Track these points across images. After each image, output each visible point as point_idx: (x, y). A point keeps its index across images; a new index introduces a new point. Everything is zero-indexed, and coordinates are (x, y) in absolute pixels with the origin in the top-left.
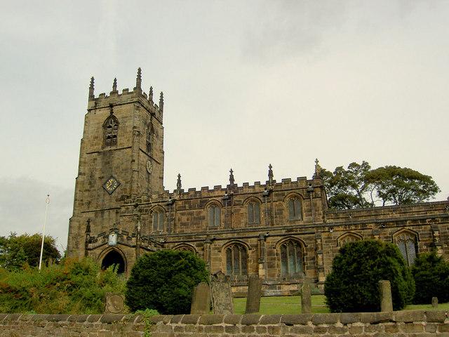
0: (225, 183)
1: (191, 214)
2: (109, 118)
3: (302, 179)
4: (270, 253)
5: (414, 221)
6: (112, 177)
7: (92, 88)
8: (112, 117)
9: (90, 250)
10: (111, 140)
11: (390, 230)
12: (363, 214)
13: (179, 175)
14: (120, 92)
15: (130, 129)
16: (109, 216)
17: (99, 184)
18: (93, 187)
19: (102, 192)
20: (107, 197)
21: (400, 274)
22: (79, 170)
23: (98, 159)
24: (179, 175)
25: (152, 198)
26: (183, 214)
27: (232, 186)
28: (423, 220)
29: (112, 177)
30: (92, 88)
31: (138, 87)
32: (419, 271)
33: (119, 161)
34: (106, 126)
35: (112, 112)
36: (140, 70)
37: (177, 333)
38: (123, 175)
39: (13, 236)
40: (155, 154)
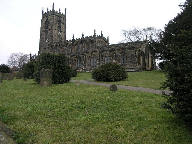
0: (81, 37)
3: (90, 37)
4: (74, 61)
5: (110, 50)
7: (43, 11)
10: (47, 27)
11: (103, 53)
12: (105, 47)
14: (49, 12)
15: (51, 23)
17: (45, 40)
20: (46, 44)
26: (62, 49)
27: (73, 39)
28: (112, 50)
30: (43, 11)
31: (53, 10)
32: (182, 45)
34: (46, 23)
35: (47, 18)
39: (178, 15)
40: (62, 30)
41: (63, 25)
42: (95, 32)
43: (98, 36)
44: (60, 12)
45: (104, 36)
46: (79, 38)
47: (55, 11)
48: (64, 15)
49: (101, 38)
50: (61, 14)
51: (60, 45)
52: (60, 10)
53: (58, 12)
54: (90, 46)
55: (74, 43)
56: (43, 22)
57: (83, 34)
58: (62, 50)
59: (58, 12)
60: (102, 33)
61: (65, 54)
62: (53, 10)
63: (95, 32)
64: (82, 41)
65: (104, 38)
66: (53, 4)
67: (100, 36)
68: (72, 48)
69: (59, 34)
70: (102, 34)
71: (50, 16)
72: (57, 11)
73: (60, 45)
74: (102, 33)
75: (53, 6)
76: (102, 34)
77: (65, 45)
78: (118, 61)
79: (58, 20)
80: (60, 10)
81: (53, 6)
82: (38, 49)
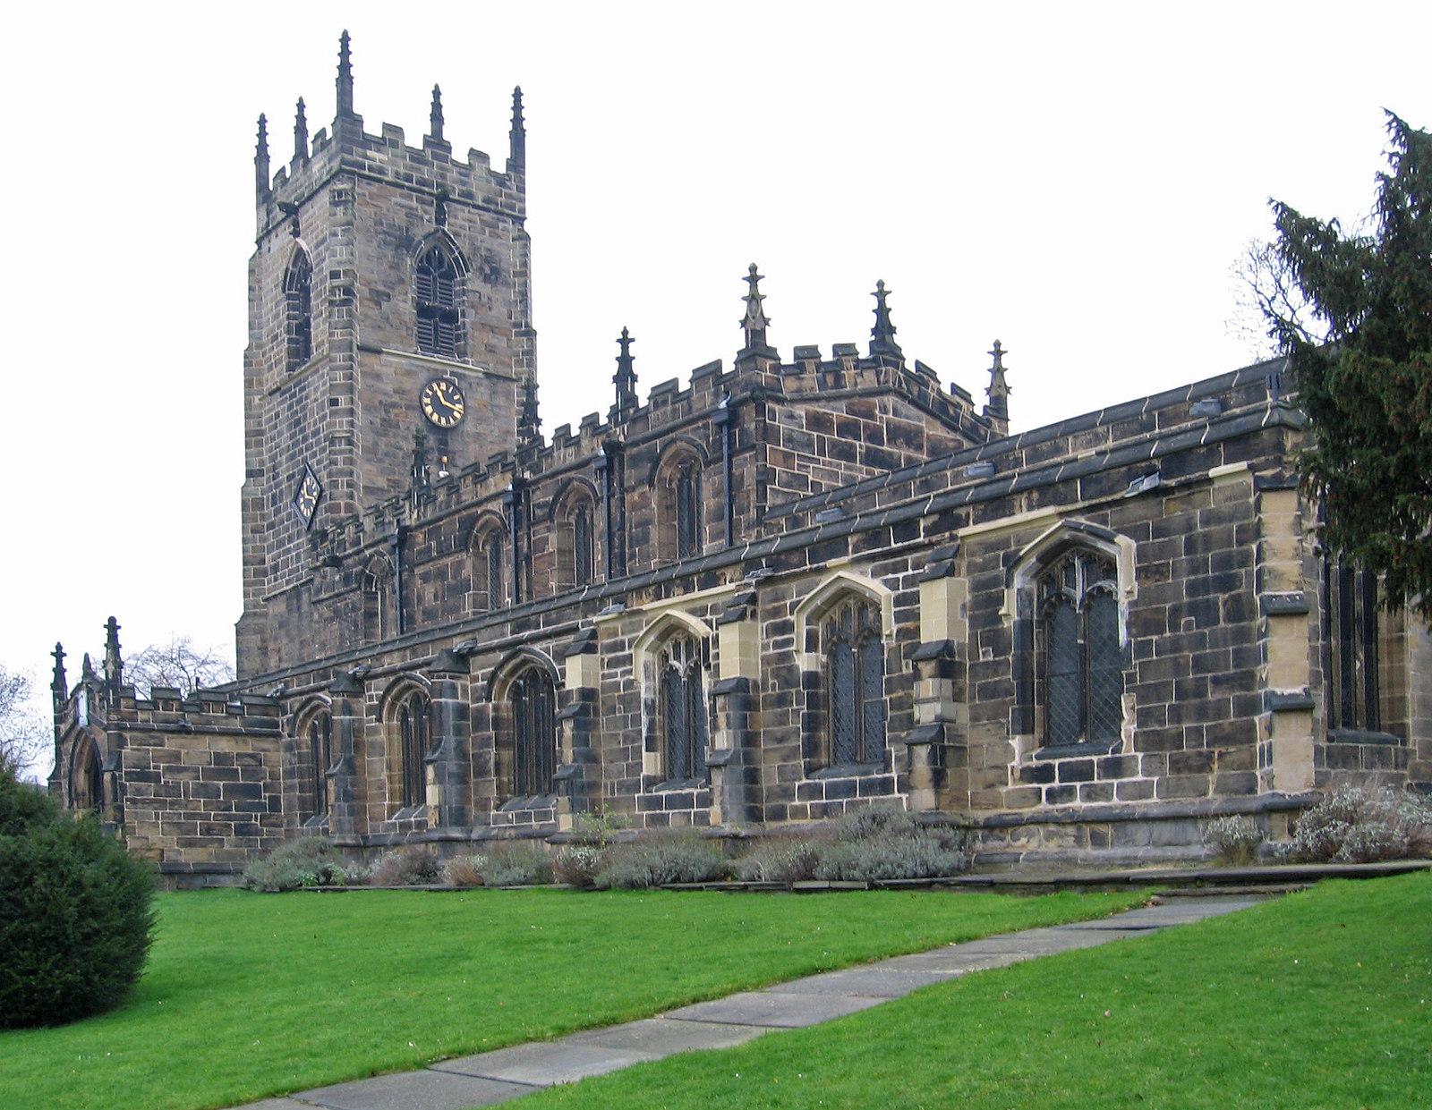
3: (708, 374)
26: (426, 578)
30: (262, 157)
31: (347, 116)
41: (486, 289)
42: (754, 299)
43: (806, 354)
44: (436, 142)
45: (913, 347)
46: (590, 422)
47: (373, 128)
48: (499, 165)
49: (869, 380)
50: (460, 155)
51: (405, 532)
52: (437, 117)
53: (414, 139)
54: (709, 502)
55: (541, 497)
56: (1175, 394)
57: (625, 361)
58: (429, 591)
59: (414, 139)
60: (882, 312)
61: (1362, 544)
62: (347, 116)
63: (754, 299)
64: (613, 449)
65: (925, 374)
66: (345, 53)
67: (844, 350)
68: (523, 561)
69: (445, 411)
70: (883, 329)
71: (324, 198)
72: (393, 133)
73: (405, 532)
74: (882, 312)
75: (345, 67)
76: (883, 329)
77: (451, 527)
78: (988, 692)
79: (418, 233)
80: (437, 117)
81: (345, 67)
82: (233, 606)
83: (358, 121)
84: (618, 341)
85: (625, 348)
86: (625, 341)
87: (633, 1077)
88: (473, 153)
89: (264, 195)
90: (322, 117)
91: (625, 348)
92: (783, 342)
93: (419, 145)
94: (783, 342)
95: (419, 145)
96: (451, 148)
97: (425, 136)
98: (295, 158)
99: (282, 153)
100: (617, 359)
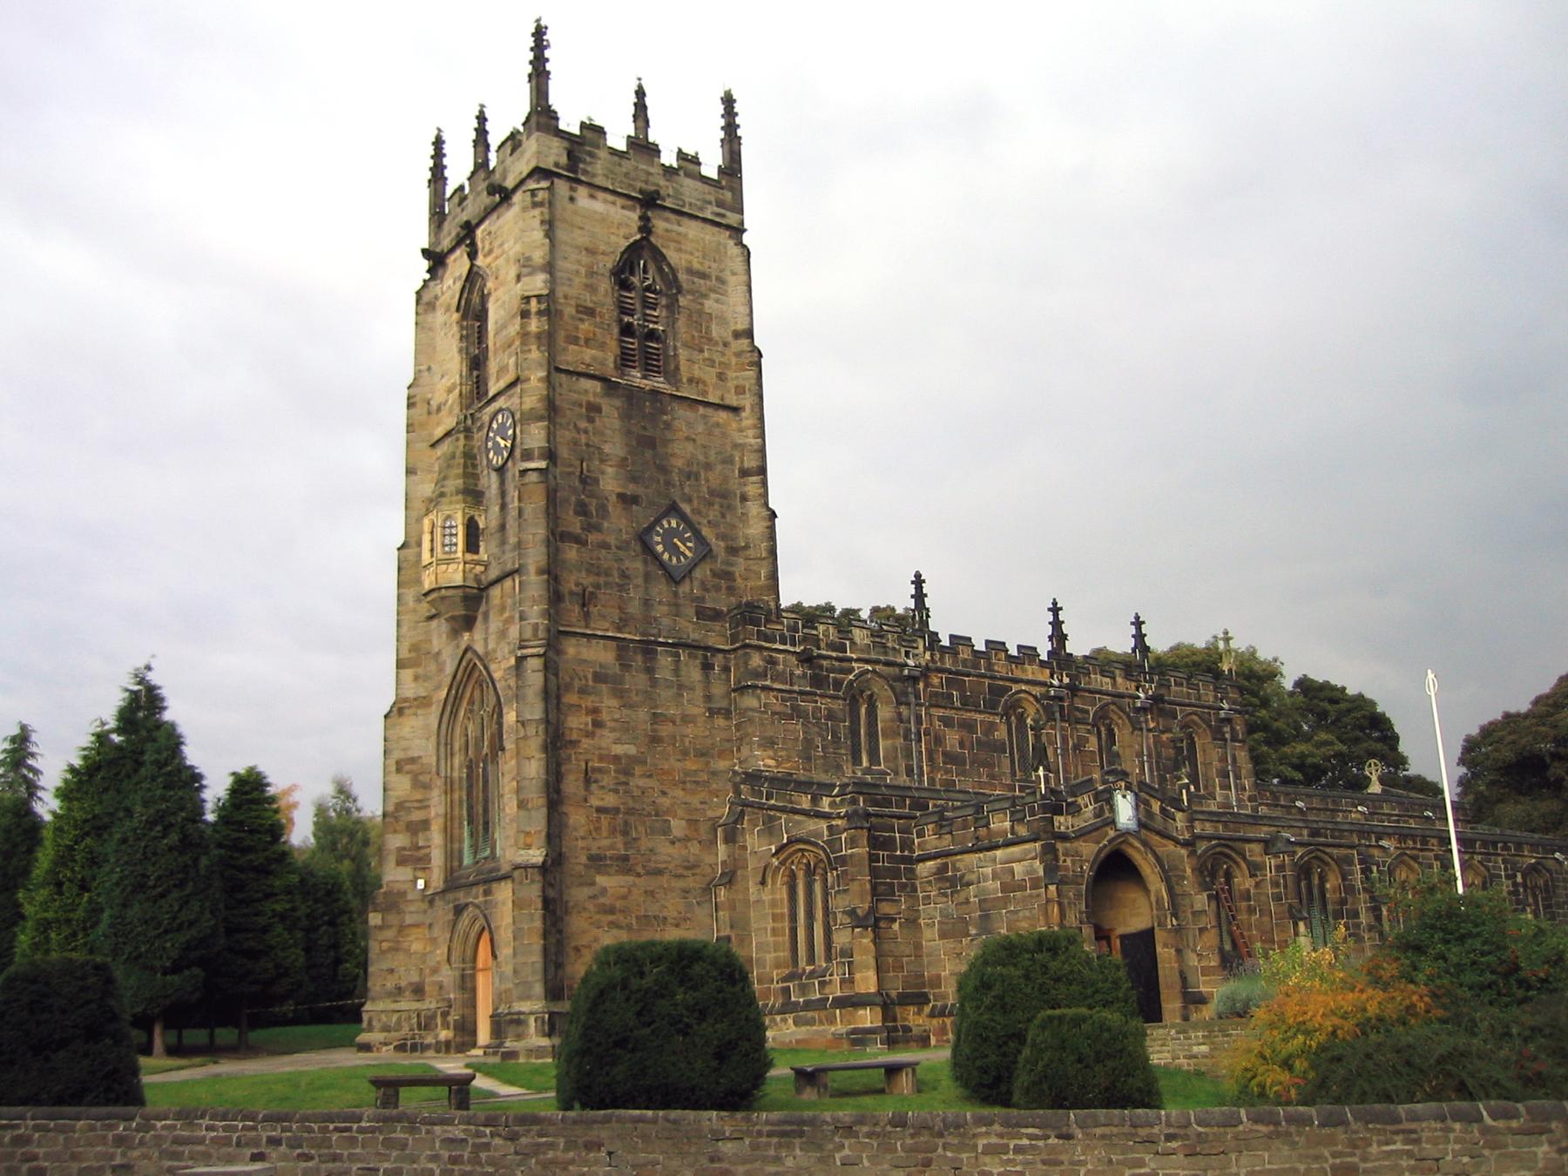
1: (968, 726)
2: (634, 251)
6: (673, 509)
8: (641, 251)
9: (1064, 837)
13: (918, 575)
16: (676, 671)
18: (598, 529)
19: (637, 566)
20: (660, 590)
21: (246, 911)
22: (764, 484)
23: (605, 408)
24: (918, 575)
25: (853, 643)
29: (673, 509)
31: (542, 115)
33: (690, 447)
35: (646, 228)
36: (728, 101)
37: (25, 1167)
38: (713, 514)
43: (797, 609)
44: (642, 146)
52: (539, 74)
62: (542, 115)
83: (554, 116)
84: (1049, 610)
85: (1056, 616)
86: (1055, 609)
87: (262, 1170)
88: (681, 155)
89: (438, 216)
90: (509, 114)
91: (1056, 616)
92: (1077, 647)
93: (714, 174)
94: (1077, 647)
95: (714, 174)
96: (659, 152)
97: (629, 137)
98: (473, 173)
99: (459, 170)
100: (912, 596)
